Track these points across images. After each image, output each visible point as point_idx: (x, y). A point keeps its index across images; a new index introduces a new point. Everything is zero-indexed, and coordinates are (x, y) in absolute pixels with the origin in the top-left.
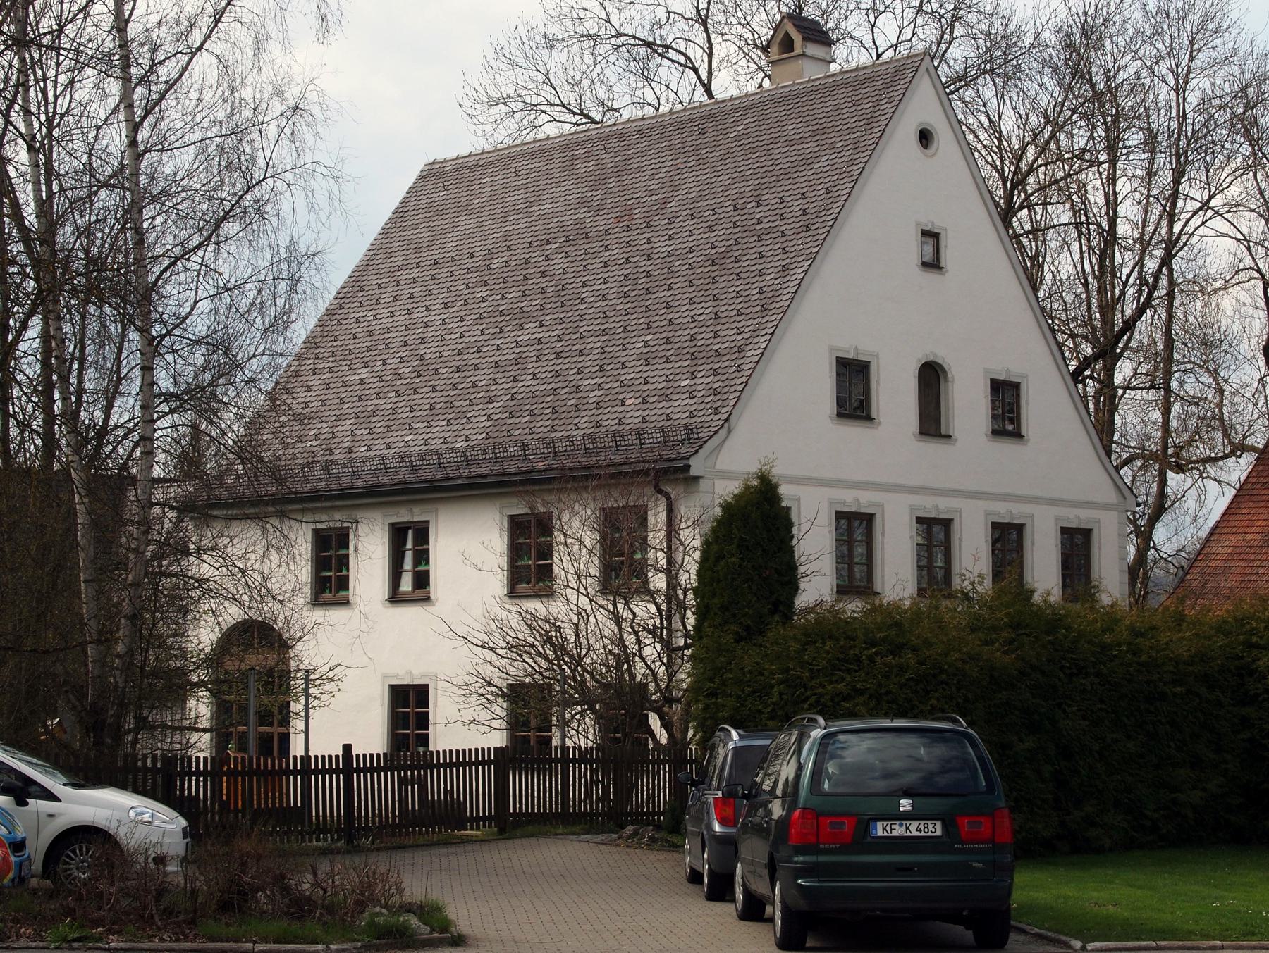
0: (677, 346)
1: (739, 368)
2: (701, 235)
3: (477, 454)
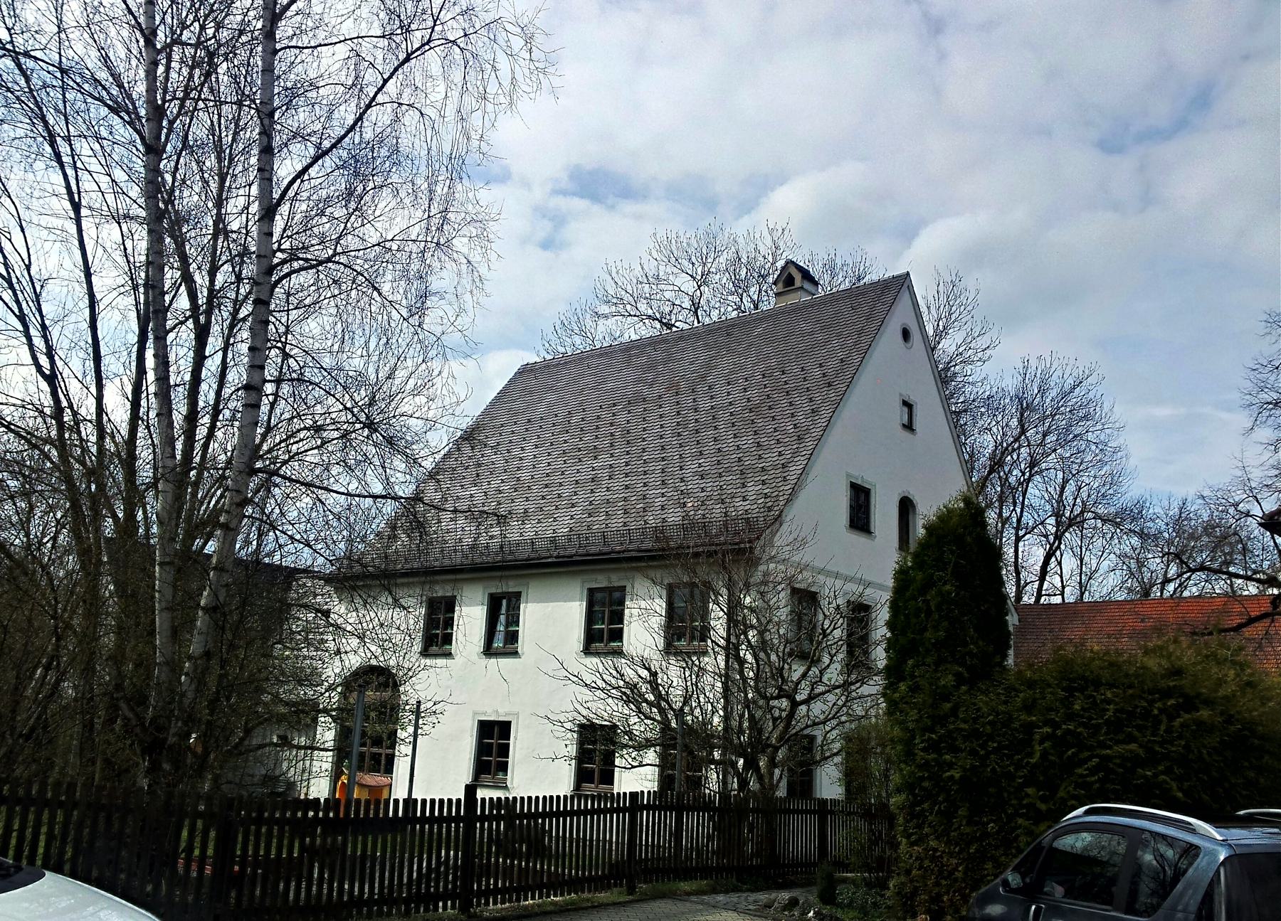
1: (785, 479)
3: (562, 541)
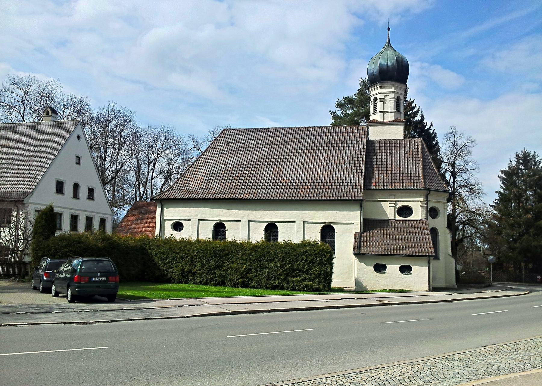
0: (20, 174)
2: (26, 151)
